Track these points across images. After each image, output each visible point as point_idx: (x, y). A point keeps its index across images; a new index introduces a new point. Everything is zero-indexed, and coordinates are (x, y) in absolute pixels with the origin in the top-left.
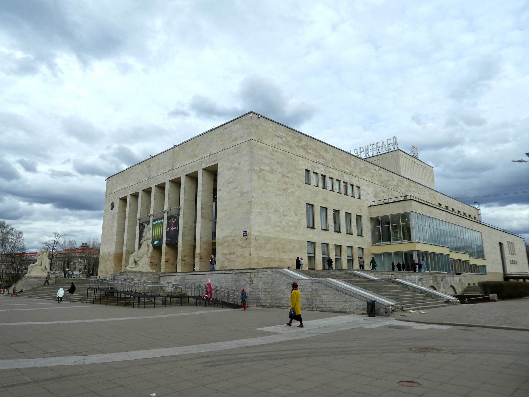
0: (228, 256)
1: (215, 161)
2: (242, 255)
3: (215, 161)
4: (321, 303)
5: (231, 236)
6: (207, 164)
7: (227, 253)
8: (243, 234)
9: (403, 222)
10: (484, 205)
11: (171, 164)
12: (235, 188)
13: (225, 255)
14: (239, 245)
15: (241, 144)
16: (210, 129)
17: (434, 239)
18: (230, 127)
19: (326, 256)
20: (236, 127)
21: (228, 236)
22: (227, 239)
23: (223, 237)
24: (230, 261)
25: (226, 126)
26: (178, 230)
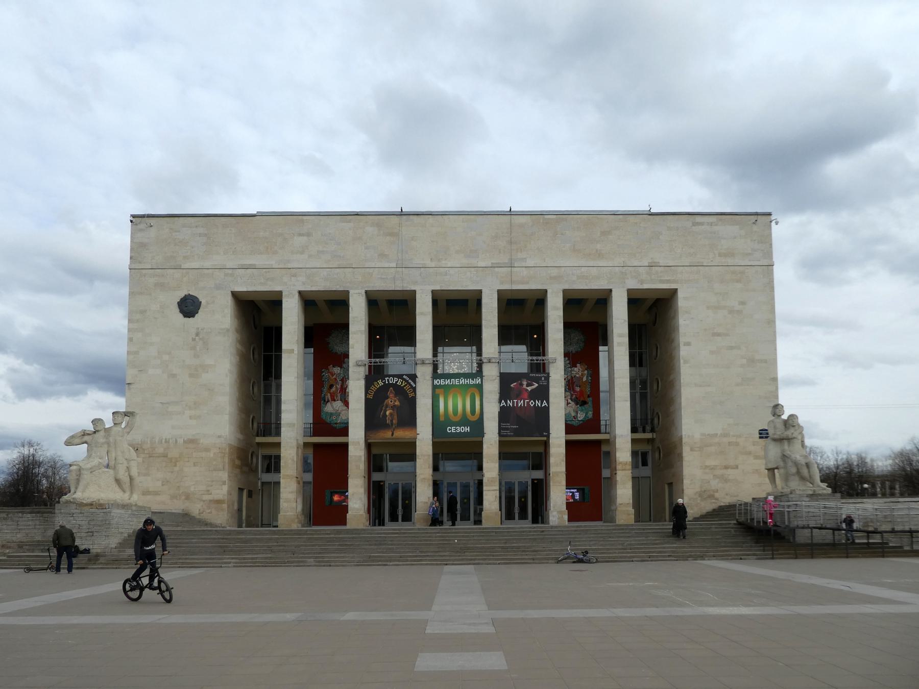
0: (719, 472)
1: (675, 282)
2: (757, 470)
3: (675, 282)
4: (818, 521)
5: (725, 435)
6: (512, 282)
7: (716, 466)
8: (760, 434)
9: (275, 352)
10: (239, 338)
11: (500, 252)
12: (731, 348)
13: (712, 469)
14: (750, 453)
15: (746, 267)
16: (644, 208)
17: (650, 407)
18: (711, 224)
19: (429, 402)
20: (728, 229)
21: (717, 434)
22: (716, 440)
23: (702, 434)
24: (726, 480)
25: (699, 219)
26: (546, 410)
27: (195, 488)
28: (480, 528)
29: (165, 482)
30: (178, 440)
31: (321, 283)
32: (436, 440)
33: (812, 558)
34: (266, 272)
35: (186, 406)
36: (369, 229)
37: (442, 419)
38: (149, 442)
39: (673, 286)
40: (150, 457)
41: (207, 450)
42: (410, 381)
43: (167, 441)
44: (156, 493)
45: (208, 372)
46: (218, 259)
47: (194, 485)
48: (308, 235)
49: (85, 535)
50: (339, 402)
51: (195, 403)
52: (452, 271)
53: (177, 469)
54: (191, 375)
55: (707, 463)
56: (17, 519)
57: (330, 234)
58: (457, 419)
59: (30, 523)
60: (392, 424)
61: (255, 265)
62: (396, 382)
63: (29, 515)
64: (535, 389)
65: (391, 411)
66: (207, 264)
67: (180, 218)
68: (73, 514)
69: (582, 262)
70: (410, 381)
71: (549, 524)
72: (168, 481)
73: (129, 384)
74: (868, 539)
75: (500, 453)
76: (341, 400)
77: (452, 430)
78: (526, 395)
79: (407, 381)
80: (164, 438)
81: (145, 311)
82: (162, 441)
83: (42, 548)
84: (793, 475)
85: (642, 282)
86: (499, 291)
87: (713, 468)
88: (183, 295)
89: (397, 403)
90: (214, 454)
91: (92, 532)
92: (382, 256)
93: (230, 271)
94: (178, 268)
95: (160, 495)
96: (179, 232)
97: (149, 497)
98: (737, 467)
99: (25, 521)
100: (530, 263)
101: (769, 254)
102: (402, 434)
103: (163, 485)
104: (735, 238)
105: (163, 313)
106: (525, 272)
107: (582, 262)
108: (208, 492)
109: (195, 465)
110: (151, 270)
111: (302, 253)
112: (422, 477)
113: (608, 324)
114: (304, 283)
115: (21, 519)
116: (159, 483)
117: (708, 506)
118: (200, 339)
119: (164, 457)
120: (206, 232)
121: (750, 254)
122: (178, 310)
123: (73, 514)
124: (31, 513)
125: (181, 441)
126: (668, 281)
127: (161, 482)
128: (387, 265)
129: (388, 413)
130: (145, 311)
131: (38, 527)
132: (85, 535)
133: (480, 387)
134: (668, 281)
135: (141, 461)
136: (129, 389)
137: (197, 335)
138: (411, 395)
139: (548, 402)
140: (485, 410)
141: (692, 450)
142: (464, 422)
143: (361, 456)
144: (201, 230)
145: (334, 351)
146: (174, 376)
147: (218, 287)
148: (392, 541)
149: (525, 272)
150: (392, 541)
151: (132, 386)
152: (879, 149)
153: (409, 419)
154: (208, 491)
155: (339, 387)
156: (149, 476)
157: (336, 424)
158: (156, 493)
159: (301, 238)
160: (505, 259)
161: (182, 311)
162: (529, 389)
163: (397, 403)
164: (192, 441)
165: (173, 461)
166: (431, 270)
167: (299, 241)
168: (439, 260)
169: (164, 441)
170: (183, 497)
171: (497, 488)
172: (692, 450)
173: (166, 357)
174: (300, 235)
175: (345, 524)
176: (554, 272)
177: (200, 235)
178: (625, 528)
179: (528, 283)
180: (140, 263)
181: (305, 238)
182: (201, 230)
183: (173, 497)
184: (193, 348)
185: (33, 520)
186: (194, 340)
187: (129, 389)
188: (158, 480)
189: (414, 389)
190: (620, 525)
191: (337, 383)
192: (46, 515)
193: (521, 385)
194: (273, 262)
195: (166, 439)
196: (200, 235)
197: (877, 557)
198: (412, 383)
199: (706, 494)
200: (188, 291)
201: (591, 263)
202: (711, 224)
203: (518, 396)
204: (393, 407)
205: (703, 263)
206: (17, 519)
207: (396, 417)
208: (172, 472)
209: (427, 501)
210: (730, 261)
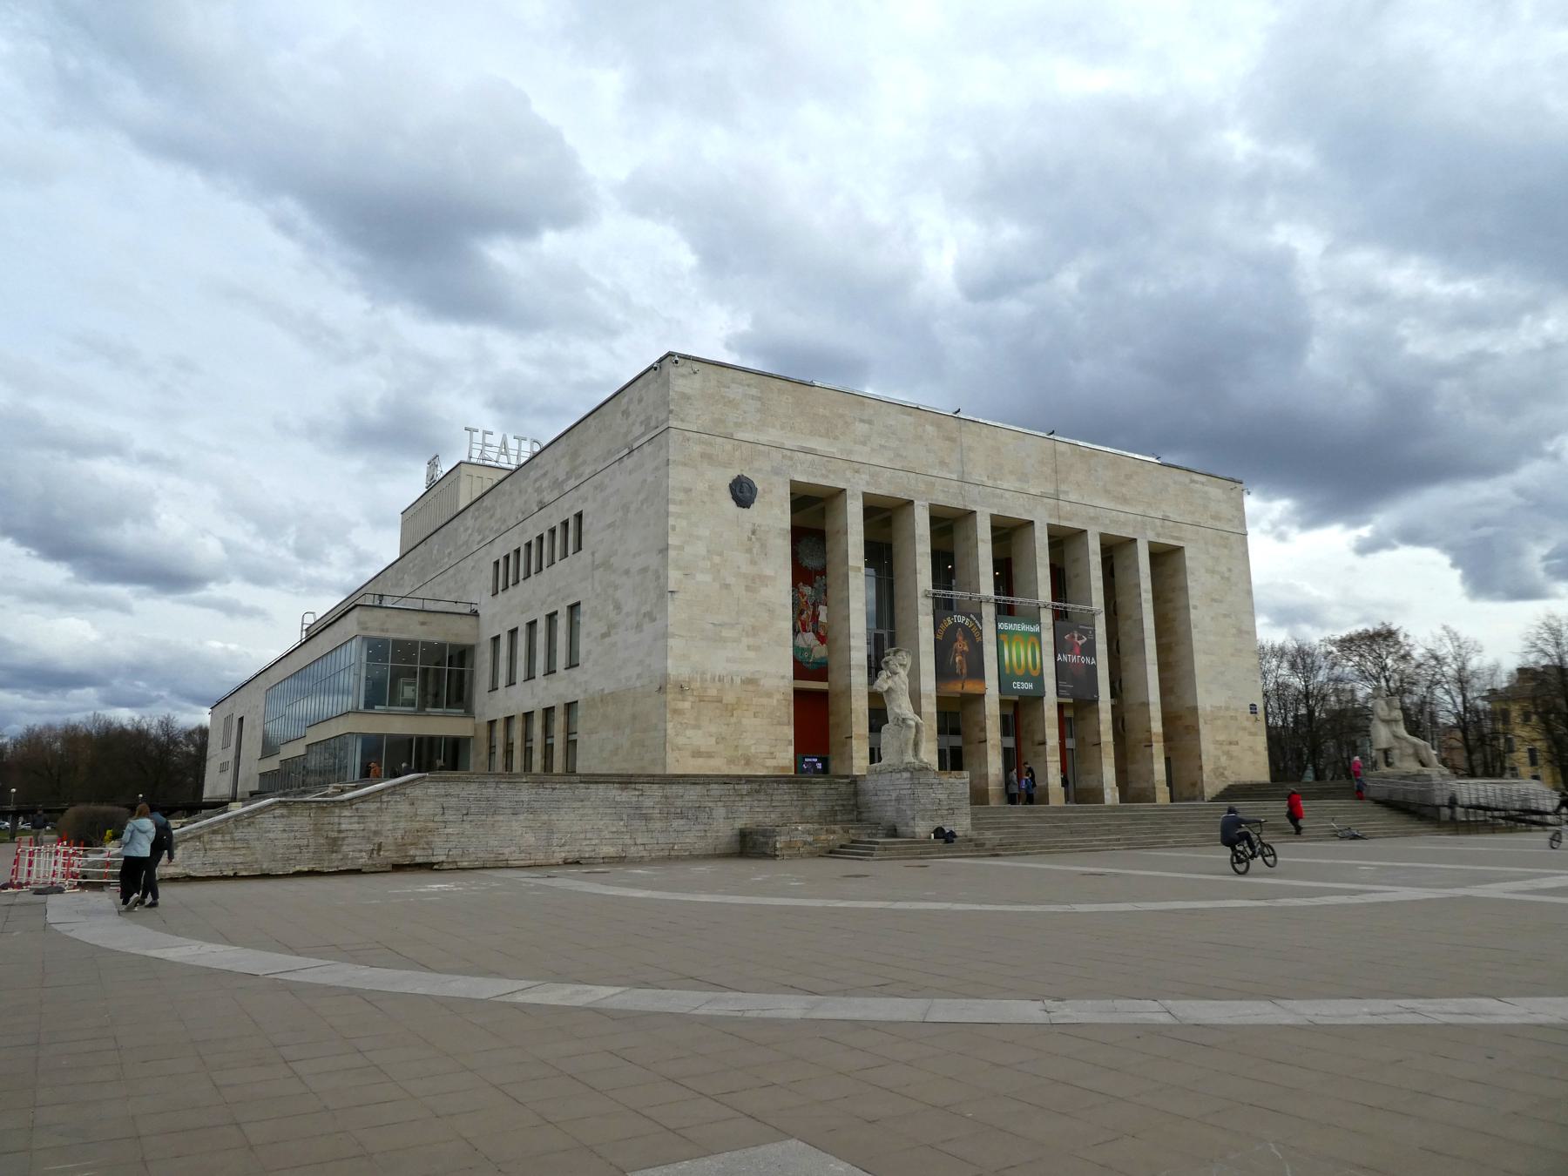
0: (1226, 748)
2: (1251, 747)
5: (1227, 708)
21: (1221, 707)
26: (1095, 666)
27: (756, 749)
28: (1154, 806)
29: (720, 739)
30: (734, 678)
31: (885, 488)
32: (1003, 697)
33: (1494, 833)
34: (827, 461)
35: (743, 630)
36: (929, 428)
37: (1008, 672)
38: (699, 680)
39: (1180, 544)
40: (700, 701)
41: (769, 695)
42: (977, 622)
43: (721, 679)
44: (709, 755)
45: (767, 586)
46: (772, 435)
47: (755, 744)
48: (870, 422)
49: (946, 812)
50: (811, 633)
51: (753, 628)
52: (1007, 495)
53: (733, 720)
54: (748, 588)
55: (1217, 739)
56: (771, 791)
57: (891, 425)
58: (1020, 672)
59: (786, 797)
60: (962, 673)
61: (815, 449)
62: (965, 622)
63: (785, 786)
64: (1085, 643)
65: (960, 657)
66: (763, 438)
67: (730, 370)
68: (932, 785)
69: (1112, 505)
70: (977, 622)
71: (1104, 803)
72: (723, 738)
73: (672, 592)
74: (1476, 817)
75: (870, 710)
76: (813, 632)
77: (1017, 685)
78: (1077, 650)
79: (974, 622)
80: (718, 674)
81: (691, 490)
82: (714, 679)
83: (869, 831)
84: (1409, 756)
85: (1158, 535)
86: (1048, 525)
87: (1221, 743)
88: (735, 476)
89: (966, 648)
90: (778, 700)
91: (952, 809)
92: (943, 463)
93: (789, 453)
94: (729, 437)
95: (713, 757)
96: (729, 388)
97: (700, 761)
98: (1237, 743)
99: (781, 794)
100: (1073, 497)
101: (1243, 523)
102: (971, 687)
103: (717, 743)
104: (1219, 501)
105: (712, 495)
106: (1068, 507)
107: (1112, 505)
108: (772, 755)
109: (755, 717)
110: (695, 434)
111: (864, 444)
112: (992, 742)
113: (895, 544)
114: (868, 484)
115: (776, 792)
116: (713, 740)
117: (1220, 786)
118: (757, 539)
119: (717, 702)
120: (759, 395)
121: (1230, 520)
122: (730, 496)
123: (932, 785)
124: (786, 783)
125: (738, 681)
126: (1177, 538)
127: (714, 739)
128: (948, 476)
129: (957, 659)
130: (691, 490)
131: (796, 803)
132: (946, 812)
133: (1038, 635)
134: (1177, 538)
135: (690, 708)
136: (673, 600)
137: (754, 532)
138: (978, 639)
139: (1095, 660)
140: (1044, 665)
141: (1206, 723)
142: (1026, 678)
143: (933, 713)
144: (754, 391)
145: (804, 565)
146: (727, 586)
147: (776, 471)
148: (1180, 818)
149: (1068, 507)
150: (1180, 818)
151: (676, 596)
152: (551, 242)
153: (978, 672)
154: (772, 753)
155: (810, 613)
156: (700, 729)
157: (808, 663)
158: (709, 755)
159: (862, 424)
160: (1050, 489)
161: (735, 498)
162: (1080, 642)
163: (966, 648)
164: (750, 681)
165: (730, 707)
166: (989, 490)
167: (862, 428)
168: (995, 480)
169: (717, 679)
170: (743, 762)
171: (1058, 758)
172: (1206, 723)
173: (717, 559)
174: (862, 421)
175: (1048, 804)
176: (1092, 511)
177: (753, 397)
178: (1113, 808)
179: (1070, 520)
180: (682, 420)
181: (867, 426)
182: (754, 391)
183: (731, 761)
184: (749, 551)
185: (789, 793)
186: (750, 539)
187: (673, 600)
188: (711, 736)
189: (981, 632)
190: (1161, 806)
191: (808, 607)
192: (805, 786)
193: (1073, 637)
194: (833, 450)
195: (720, 676)
196: (753, 397)
197: (1504, 832)
198: (979, 625)
199: (1219, 772)
200: (742, 470)
201: (1120, 508)
202: (1203, 484)
203: (1071, 651)
204: (962, 653)
205: (594, 419)
206: (771, 791)
207: (965, 666)
208: (728, 725)
209: (997, 773)
210: (1219, 525)
